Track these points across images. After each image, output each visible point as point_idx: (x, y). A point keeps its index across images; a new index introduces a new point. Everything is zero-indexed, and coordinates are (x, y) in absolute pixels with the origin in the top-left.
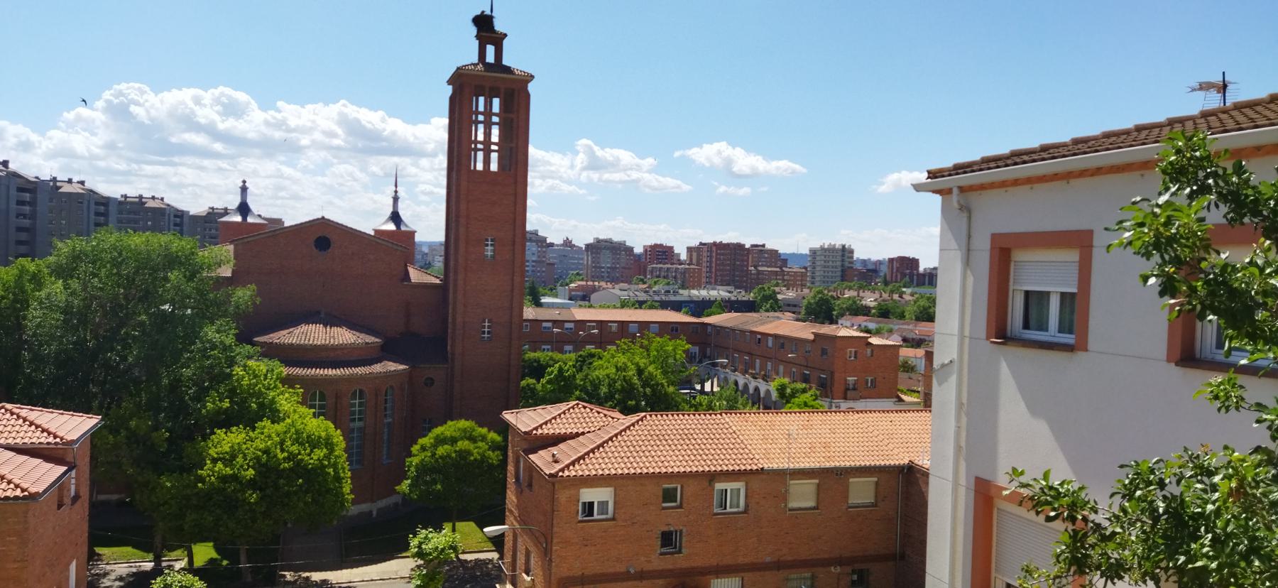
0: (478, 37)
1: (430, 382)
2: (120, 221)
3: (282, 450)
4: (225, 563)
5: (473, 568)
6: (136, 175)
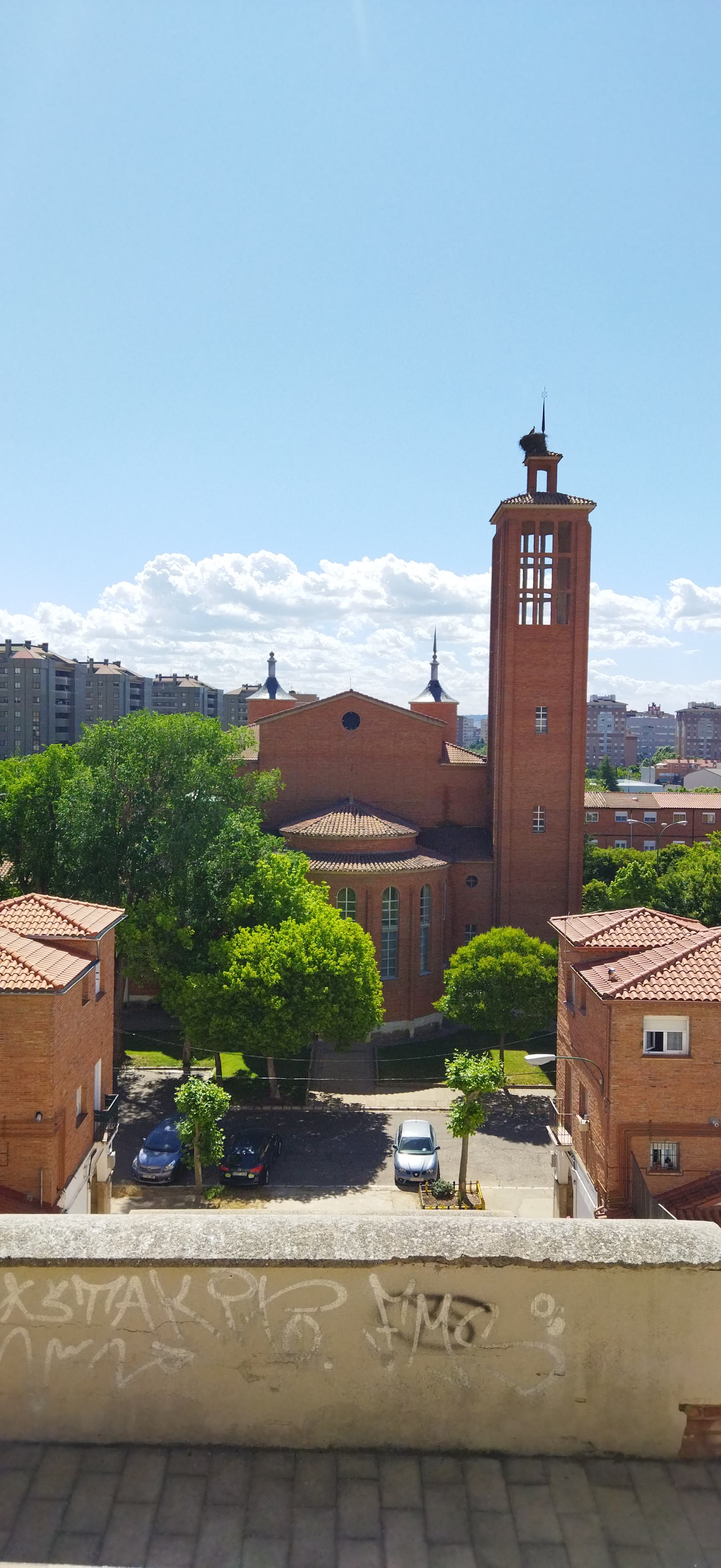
0: (526, 462)
1: (473, 881)
2: (155, 704)
3: (308, 954)
4: (254, 1076)
5: (525, 1106)
6: (174, 653)
